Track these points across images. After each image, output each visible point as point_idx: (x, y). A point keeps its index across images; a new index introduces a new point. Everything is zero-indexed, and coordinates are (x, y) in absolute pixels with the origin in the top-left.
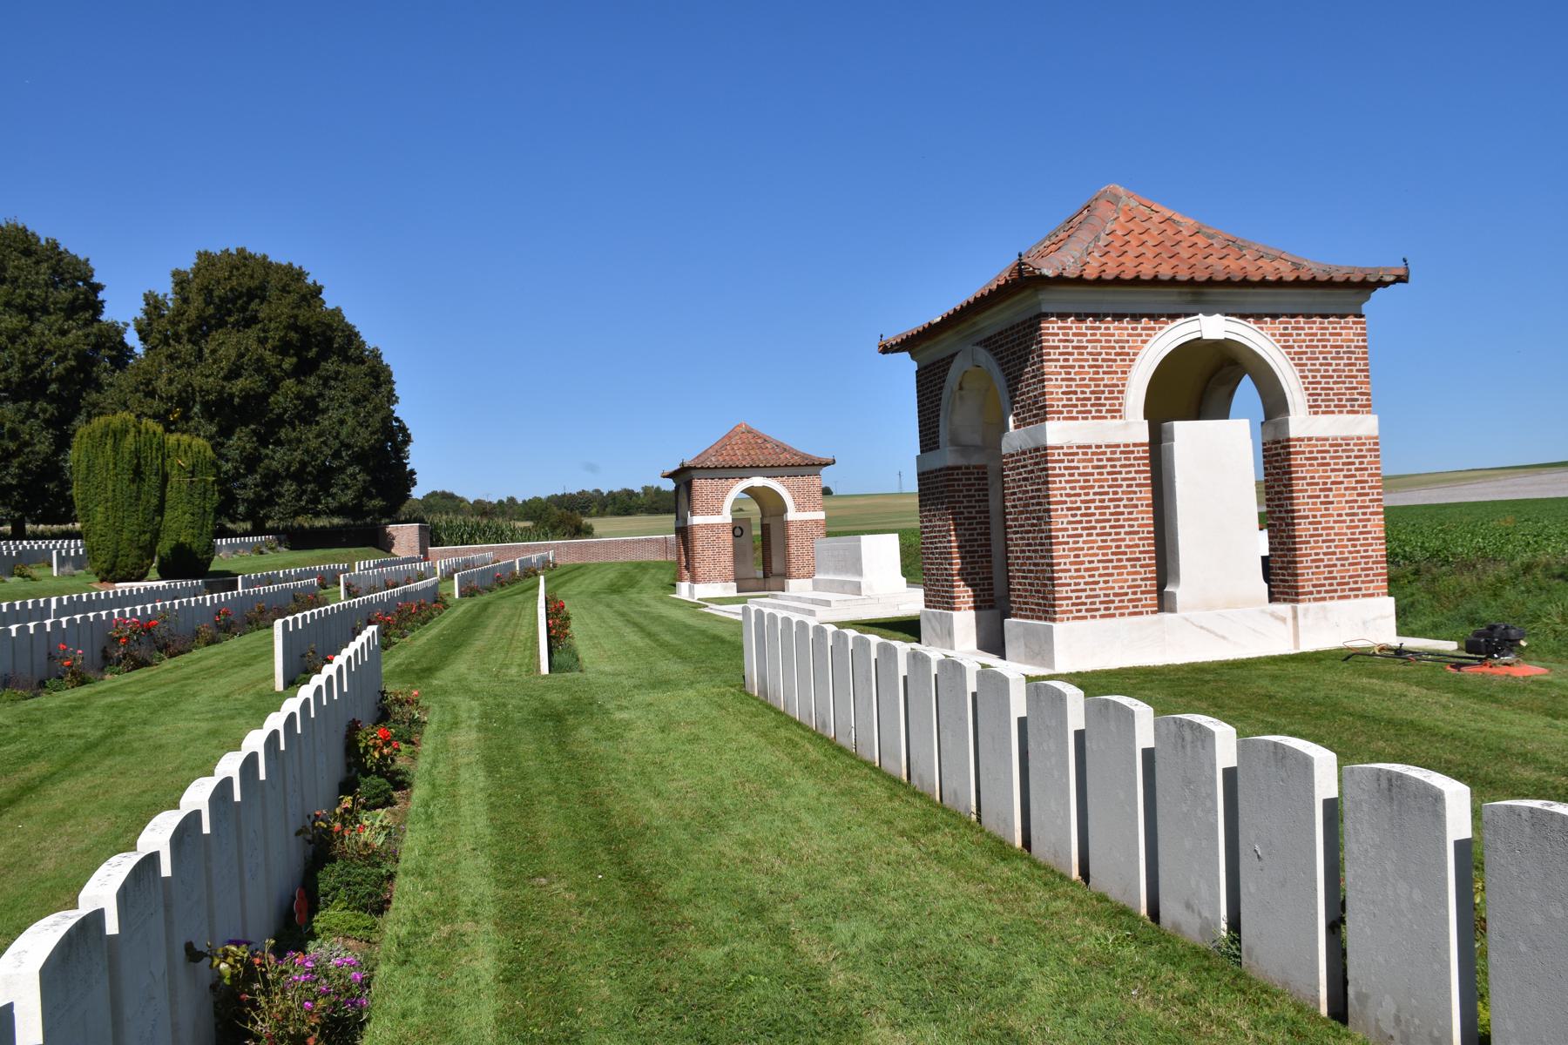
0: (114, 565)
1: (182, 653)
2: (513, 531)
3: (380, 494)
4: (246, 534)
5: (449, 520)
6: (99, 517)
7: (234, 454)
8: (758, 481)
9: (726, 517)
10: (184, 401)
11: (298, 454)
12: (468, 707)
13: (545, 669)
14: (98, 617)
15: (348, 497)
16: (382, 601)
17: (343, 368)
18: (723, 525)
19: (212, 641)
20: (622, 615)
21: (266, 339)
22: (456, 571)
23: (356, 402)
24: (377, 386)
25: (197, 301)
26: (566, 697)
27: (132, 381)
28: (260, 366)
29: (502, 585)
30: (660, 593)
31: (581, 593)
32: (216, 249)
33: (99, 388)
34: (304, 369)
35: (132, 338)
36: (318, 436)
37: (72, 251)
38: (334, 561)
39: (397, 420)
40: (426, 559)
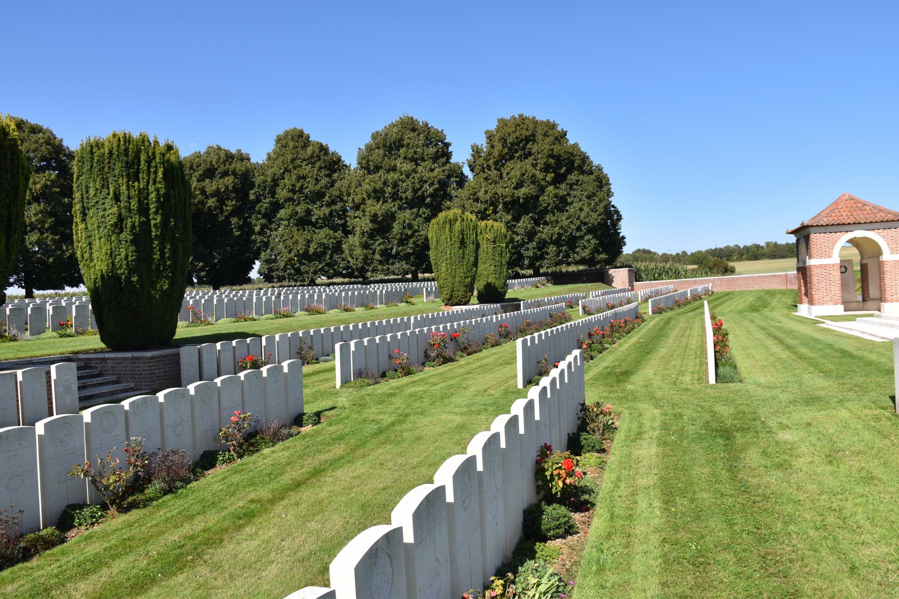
0: (452, 296)
1: (475, 352)
2: (686, 271)
3: (605, 251)
4: (530, 276)
5: (646, 266)
6: (444, 269)
7: (521, 231)
8: (859, 234)
9: (835, 260)
10: (493, 203)
11: (557, 229)
12: (651, 414)
13: (712, 379)
14: (421, 331)
15: (586, 253)
16: (599, 320)
17: (581, 177)
18: (833, 265)
19: (496, 344)
20: (763, 329)
21: (537, 164)
22: (650, 297)
23: (589, 197)
24: (601, 187)
25: (498, 146)
26: (732, 411)
27: (467, 193)
28: (534, 180)
29: (679, 306)
30: (786, 311)
31: (731, 311)
32: (507, 116)
33: (451, 199)
34: (558, 180)
35: (466, 171)
36: (567, 218)
37: (435, 127)
38: (578, 291)
39: (613, 206)
40: (633, 289)
